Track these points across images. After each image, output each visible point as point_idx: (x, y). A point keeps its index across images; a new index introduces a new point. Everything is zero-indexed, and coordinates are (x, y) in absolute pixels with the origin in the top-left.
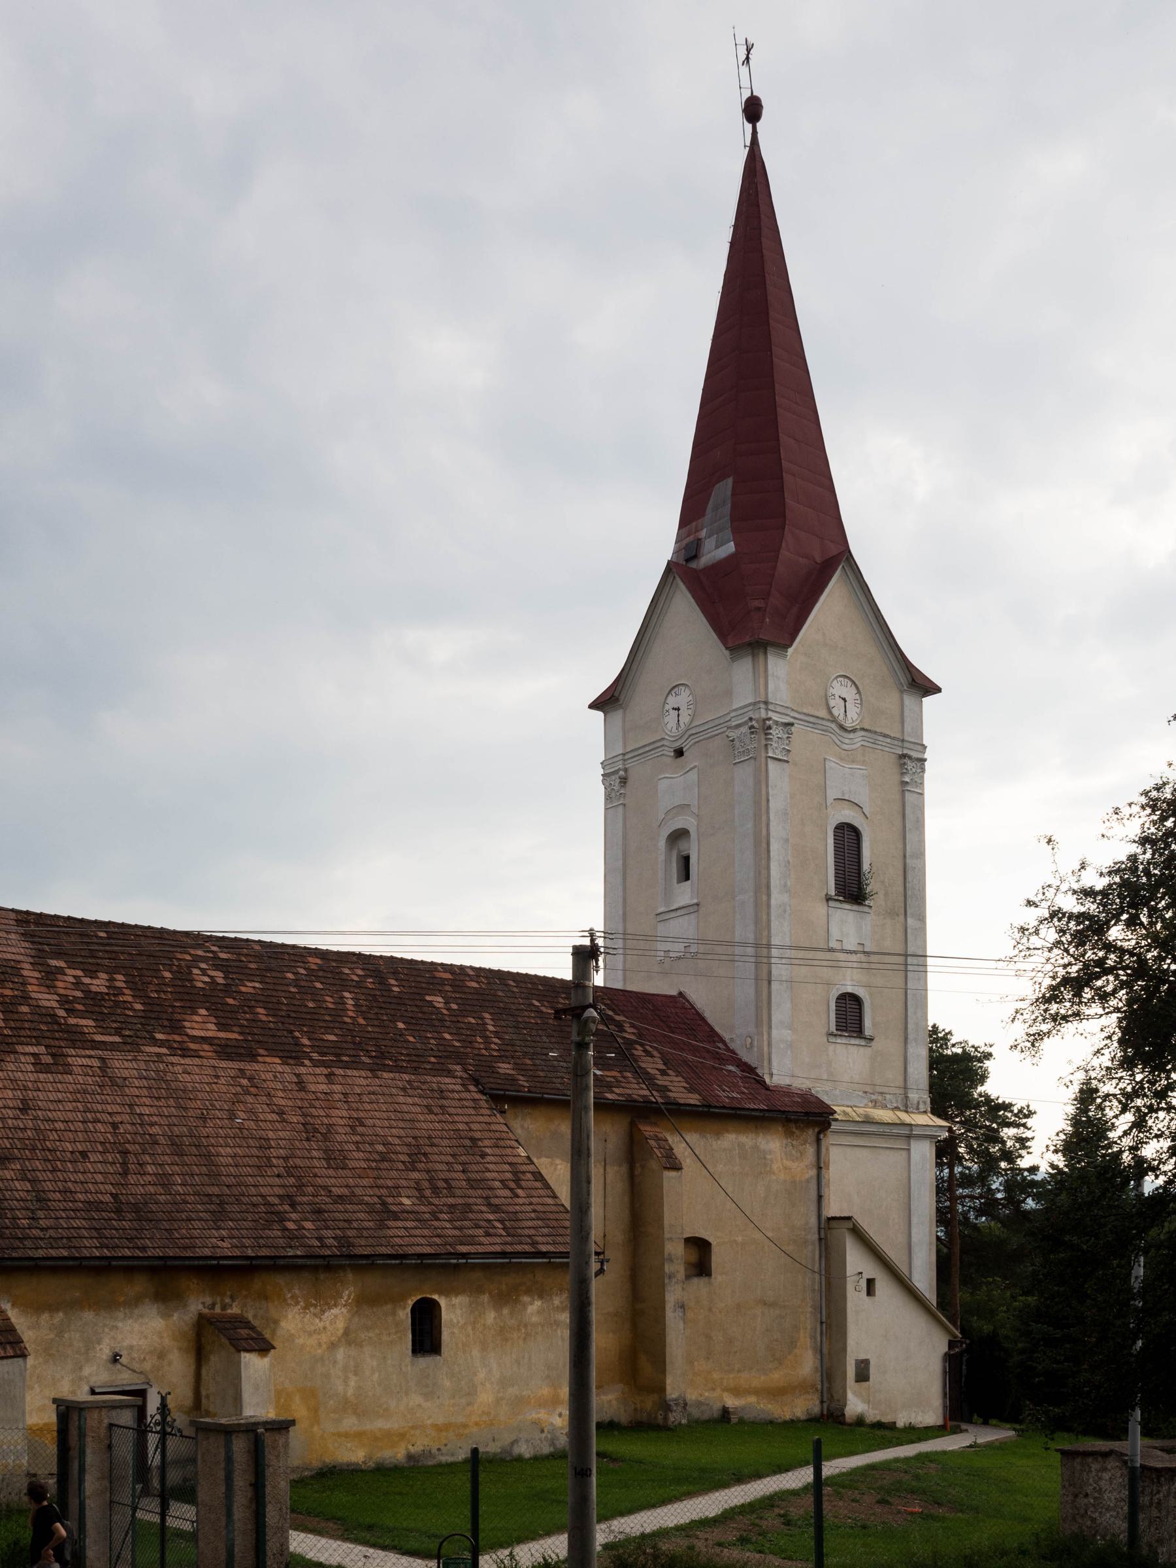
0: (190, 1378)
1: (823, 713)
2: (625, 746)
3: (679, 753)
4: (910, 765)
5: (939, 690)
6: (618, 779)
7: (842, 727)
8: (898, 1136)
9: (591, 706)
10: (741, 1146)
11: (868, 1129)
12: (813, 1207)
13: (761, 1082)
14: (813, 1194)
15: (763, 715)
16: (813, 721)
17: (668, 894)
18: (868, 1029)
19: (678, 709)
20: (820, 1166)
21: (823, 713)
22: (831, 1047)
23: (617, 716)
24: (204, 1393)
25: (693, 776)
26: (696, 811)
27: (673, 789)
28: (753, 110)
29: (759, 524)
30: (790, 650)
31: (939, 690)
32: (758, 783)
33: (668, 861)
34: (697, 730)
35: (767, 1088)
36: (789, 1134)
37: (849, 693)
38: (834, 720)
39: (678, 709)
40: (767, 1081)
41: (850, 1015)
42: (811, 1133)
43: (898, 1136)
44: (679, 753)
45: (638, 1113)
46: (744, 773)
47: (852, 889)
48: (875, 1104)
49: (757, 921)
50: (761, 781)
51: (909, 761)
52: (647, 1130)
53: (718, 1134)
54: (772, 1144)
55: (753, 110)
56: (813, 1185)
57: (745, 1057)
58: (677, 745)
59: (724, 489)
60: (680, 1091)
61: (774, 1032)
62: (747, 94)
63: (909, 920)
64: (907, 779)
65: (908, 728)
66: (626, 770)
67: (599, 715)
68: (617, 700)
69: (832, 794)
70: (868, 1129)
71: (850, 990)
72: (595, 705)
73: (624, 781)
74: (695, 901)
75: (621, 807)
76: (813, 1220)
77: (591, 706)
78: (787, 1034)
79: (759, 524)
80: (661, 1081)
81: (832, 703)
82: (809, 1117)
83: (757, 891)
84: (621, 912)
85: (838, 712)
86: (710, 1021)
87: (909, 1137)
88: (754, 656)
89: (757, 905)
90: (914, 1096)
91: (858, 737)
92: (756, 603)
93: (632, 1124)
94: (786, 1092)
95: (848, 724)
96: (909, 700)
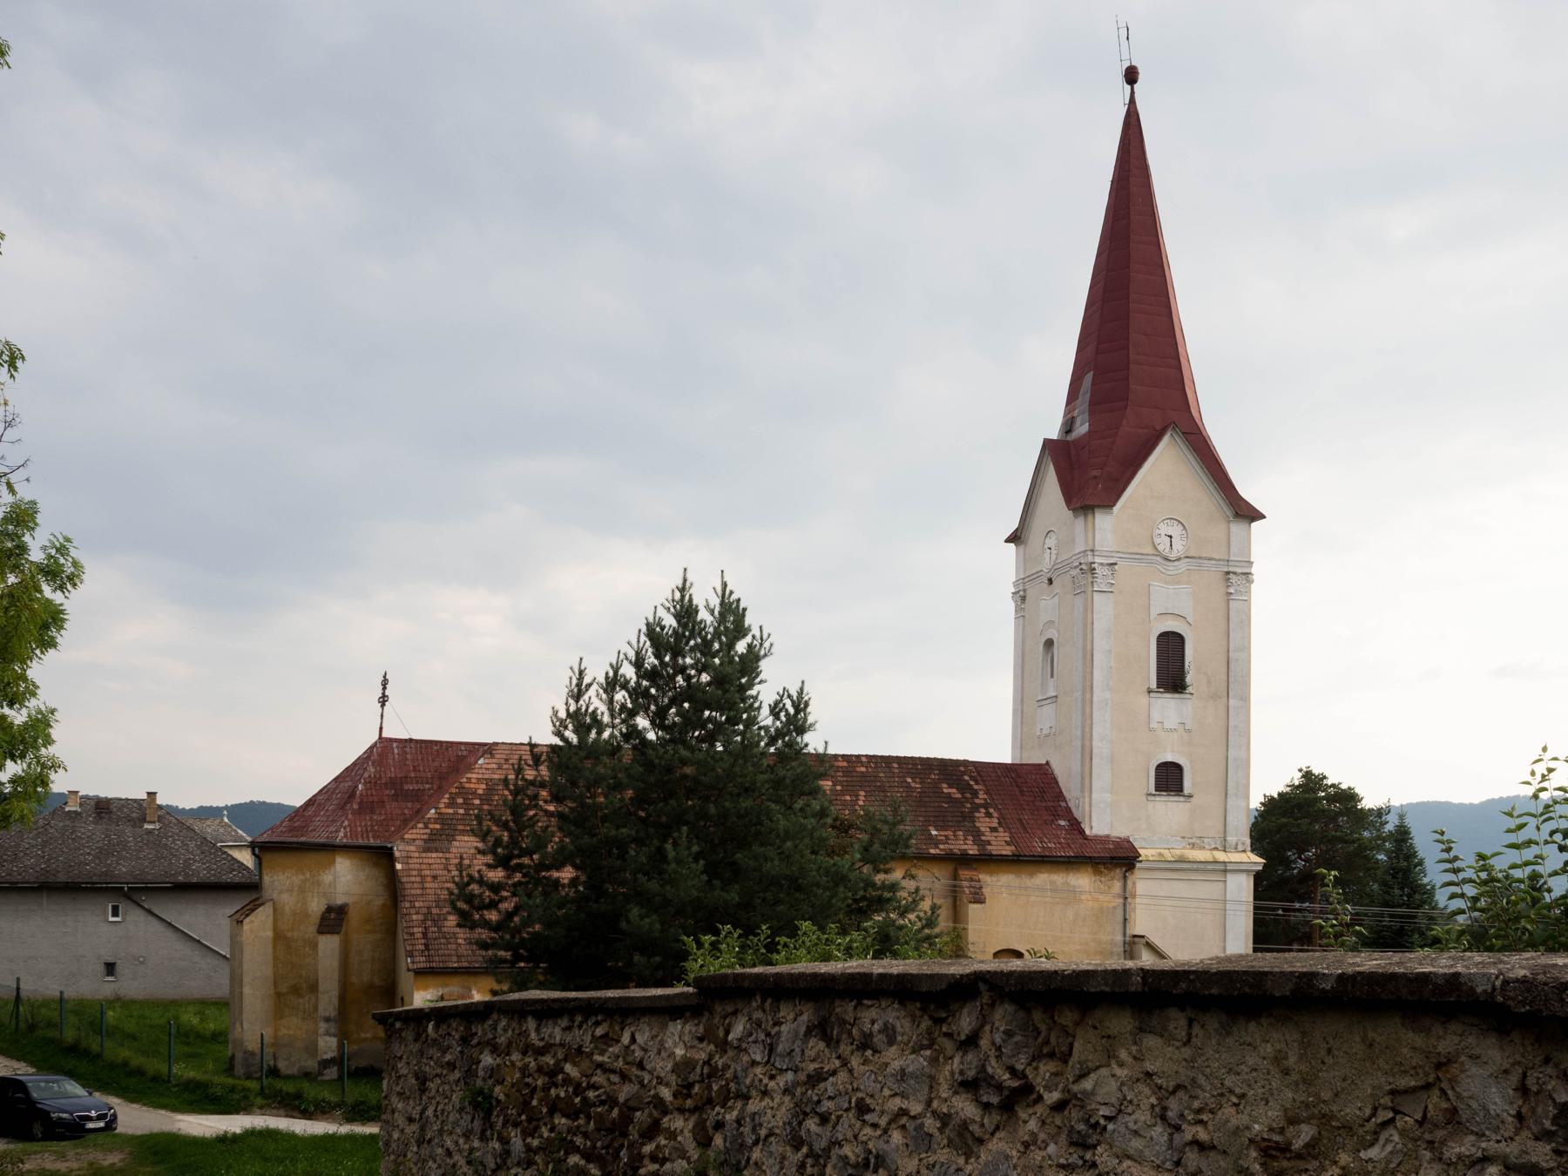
1: (1149, 550)
3: (1050, 581)
4: (1234, 579)
5: (1263, 517)
7: (1166, 559)
8: (1214, 871)
10: (1053, 883)
11: (1179, 867)
12: (1119, 928)
13: (1082, 832)
14: (1120, 918)
15: (1090, 559)
16: (1138, 557)
17: (1044, 685)
18: (1186, 791)
20: (1126, 897)
21: (1149, 550)
22: (1151, 805)
27: (1047, 605)
28: (1131, 76)
29: (1129, 392)
30: (1116, 509)
31: (1263, 517)
32: (1086, 610)
35: (1085, 838)
36: (1097, 872)
37: (1176, 531)
38: (1159, 554)
40: (1088, 832)
41: (1169, 778)
42: (1119, 872)
43: (1214, 871)
44: (1050, 581)
45: (961, 861)
46: (1079, 601)
47: (1172, 678)
48: (1193, 846)
49: (1083, 713)
50: (1088, 608)
51: (1234, 577)
52: (964, 873)
53: (1032, 875)
54: (1082, 881)
55: (1131, 76)
56: (1120, 912)
57: (1077, 814)
59: (1089, 377)
60: (1000, 844)
61: (1094, 795)
62: (1127, 64)
63: (1231, 701)
64: (1232, 590)
65: (1234, 549)
67: (1012, 546)
69: (1154, 611)
70: (1179, 867)
71: (1170, 759)
73: (1023, 599)
76: (1119, 938)
78: (1108, 797)
79: (1129, 392)
80: (988, 836)
81: (1157, 541)
82: (1119, 859)
83: (1084, 691)
85: (1163, 545)
87: (1225, 871)
88: (1086, 515)
89: (1084, 700)
90: (1231, 839)
91: (1183, 566)
92: (1095, 473)
93: (956, 870)
94: (1103, 840)
95: (1173, 556)
96: (1237, 528)
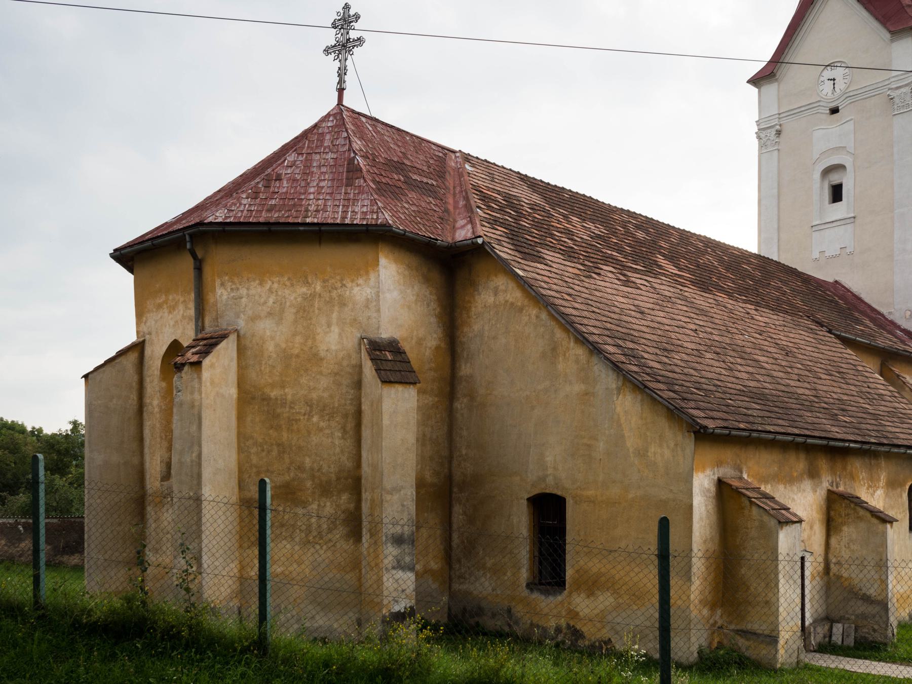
0: (823, 543)
2: (779, 108)
6: (771, 134)
9: (748, 82)
19: (834, 80)
23: (771, 89)
24: (256, 512)
25: (850, 126)
26: (852, 151)
27: (827, 139)
33: (822, 188)
34: (851, 94)
39: (834, 80)
58: (833, 105)
66: (780, 125)
68: (775, 75)
72: (128, 256)
74: (852, 215)
75: (776, 152)
77: (748, 82)
84: (776, 226)
86: (866, 300)
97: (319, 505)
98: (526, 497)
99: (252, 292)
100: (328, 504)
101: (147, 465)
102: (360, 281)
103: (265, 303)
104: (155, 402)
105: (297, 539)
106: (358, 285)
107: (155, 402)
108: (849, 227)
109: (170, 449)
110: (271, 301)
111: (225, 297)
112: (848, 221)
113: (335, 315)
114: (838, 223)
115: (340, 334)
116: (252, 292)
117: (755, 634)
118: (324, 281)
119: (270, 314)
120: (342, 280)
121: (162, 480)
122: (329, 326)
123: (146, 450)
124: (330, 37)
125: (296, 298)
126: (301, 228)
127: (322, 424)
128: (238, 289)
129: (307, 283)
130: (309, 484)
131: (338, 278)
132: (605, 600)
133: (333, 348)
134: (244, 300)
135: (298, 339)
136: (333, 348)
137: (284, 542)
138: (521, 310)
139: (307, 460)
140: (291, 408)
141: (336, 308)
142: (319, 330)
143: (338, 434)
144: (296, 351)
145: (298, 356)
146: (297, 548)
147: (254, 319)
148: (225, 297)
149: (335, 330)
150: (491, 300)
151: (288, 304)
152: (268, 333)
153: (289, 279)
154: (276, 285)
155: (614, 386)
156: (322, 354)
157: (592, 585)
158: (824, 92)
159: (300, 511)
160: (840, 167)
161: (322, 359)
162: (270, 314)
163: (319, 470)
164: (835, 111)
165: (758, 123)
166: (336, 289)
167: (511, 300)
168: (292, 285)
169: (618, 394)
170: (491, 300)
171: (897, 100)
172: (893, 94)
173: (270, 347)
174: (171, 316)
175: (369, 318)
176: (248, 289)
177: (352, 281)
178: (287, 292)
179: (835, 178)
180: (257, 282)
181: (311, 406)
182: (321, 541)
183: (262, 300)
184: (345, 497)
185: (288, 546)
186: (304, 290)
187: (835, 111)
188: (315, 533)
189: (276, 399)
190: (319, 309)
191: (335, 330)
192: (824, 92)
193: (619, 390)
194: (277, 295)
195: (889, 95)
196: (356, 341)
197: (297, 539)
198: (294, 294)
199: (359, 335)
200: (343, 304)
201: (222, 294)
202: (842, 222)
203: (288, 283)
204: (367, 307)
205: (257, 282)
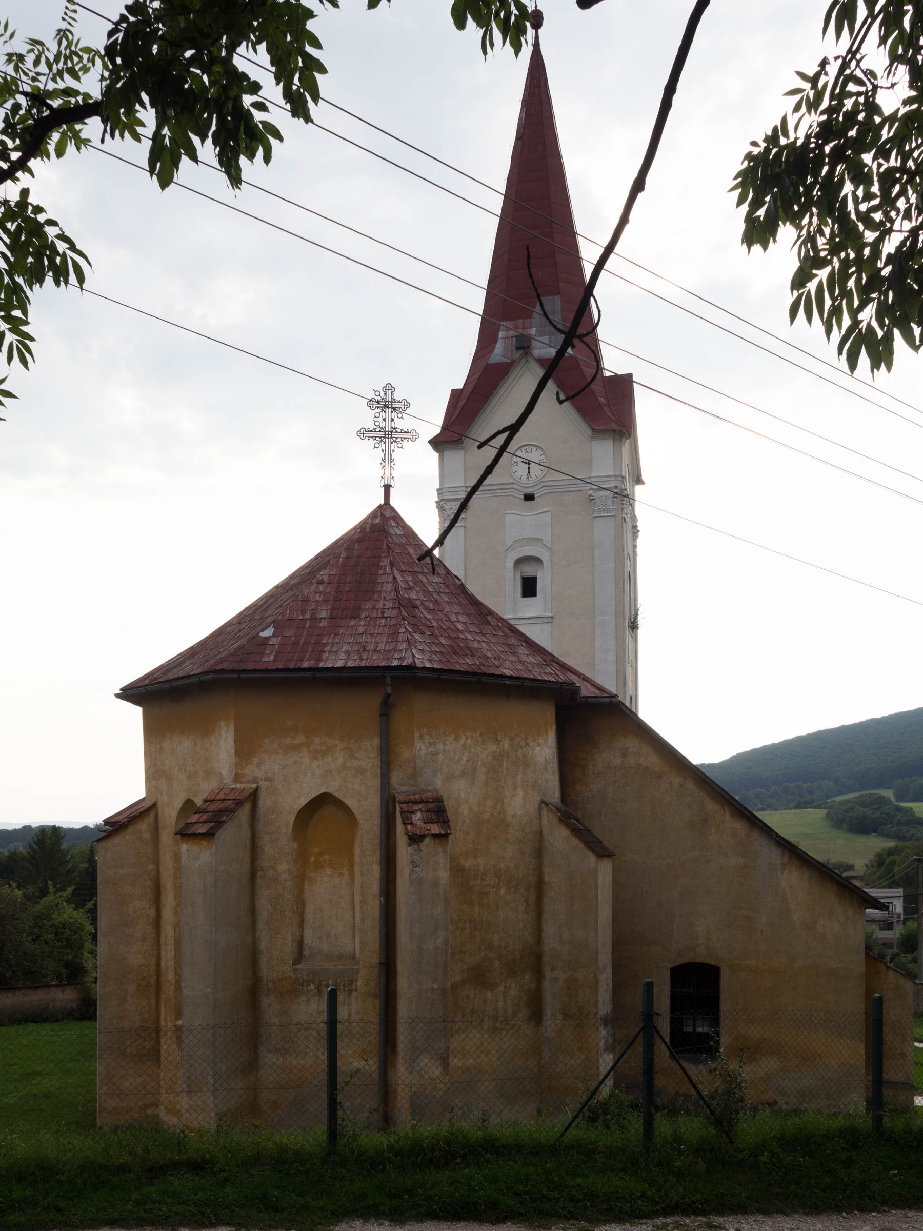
2: (465, 480)
33: (514, 579)
58: (529, 491)
68: (462, 443)
74: (550, 614)
75: (463, 529)
97: (505, 987)
98: (670, 966)
99: (448, 747)
100: (513, 985)
101: (263, 944)
102: (541, 741)
103: (459, 760)
104: (282, 867)
105: (486, 1027)
106: (539, 745)
107: (282, 867)
108: (547, 627)
109: (301, 925)
110: (465, 758)
111: (423, 752)
112: (546, 620)
113: (519, 777)
114: (535, 621)
115: (524, 798)
116: (448, 747)
117: (892, 1083)
118: (512, 739)
119: (464, 774)
120: (526, 738)
121: (294, 964)
122: (515, 789)
123: (261, 926)
124: (368, 418)
125: (487, 757)
126: (507, 682)
127: (508, 897)
128: (435, 743)
129: (497, 741)
130: (497, 964)
131: (523, 735)
132: (769, 1064)
133: (519, 813)
134: (440, 756)
135: (489, 802)
136: (519, 813)
137: (474, 1031)
138: (659, 776)
139: (496, 938)
140: (483, 880)
141: (521, 769)
142: (507, 793)
143: (522, 907)
144: (487, 816)
145: (488, 821)
146: (486, 1036)
147: (450, 778)
148: (423, 752)
149: (520, 792)
150: (618, 760)
151: (480, 762)
152: (463, 796)
153: (481, 734)
154: (469, 741)
155: (779, 862)
156: (509, 819)
157: (748, 1050)
158: (518, 475)
159: (489, 995)
160: (537, 560)
161: (508, 825)
162: (464, 774)
163: (506, 948)
164: (529, 497)
165: (440, 492)
166: (521, 748)
167: (645, 764)
168: (484, 742)
169: (784, 869)
170: (618, 760)
171: (598, 502)
172: (595, 495)
173: (465, 811)
174: (316, 763)
175: (547, 780)
176: (444, 744)
177: (534, 740)
178: (479, 748)
179: (529, 571)
180: (453, 736)
181: (499, 878)
182: (507, 1027)
183: (457, 757)
184: (527, 976)
185: (478, 1035)
186: (494, 747)
187: (529, 497)
188: (502, 1019)
189: (470, 870)
190: (507, 769)
191: (520, 792)
192: (518, 475)
193: (784, 867)
194: (470, 753)
195: (590, 495)
196: (536, 805)
197: (486, 1027)
198: (486, 751)
199: (539, 799)
200: (527, 765)
201: (420, 749)
202: (538, 621)
203: (480, 739)
204: (546, 768)
205: (453, 736)
